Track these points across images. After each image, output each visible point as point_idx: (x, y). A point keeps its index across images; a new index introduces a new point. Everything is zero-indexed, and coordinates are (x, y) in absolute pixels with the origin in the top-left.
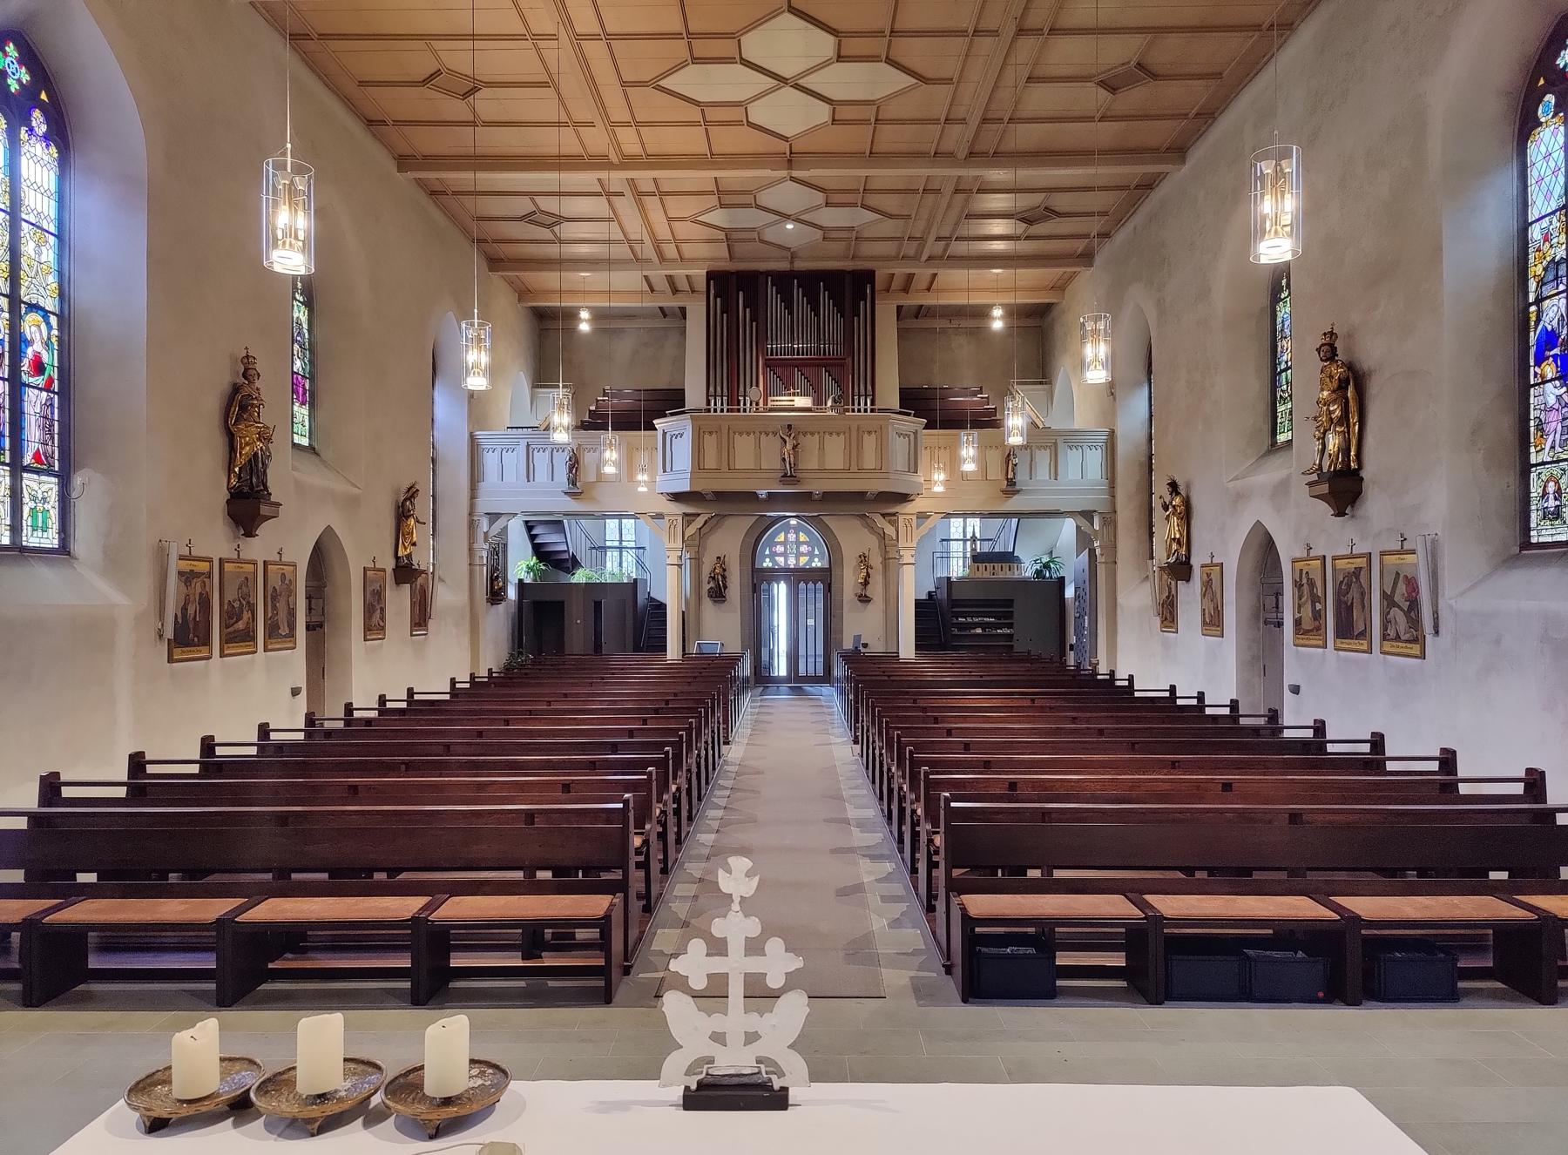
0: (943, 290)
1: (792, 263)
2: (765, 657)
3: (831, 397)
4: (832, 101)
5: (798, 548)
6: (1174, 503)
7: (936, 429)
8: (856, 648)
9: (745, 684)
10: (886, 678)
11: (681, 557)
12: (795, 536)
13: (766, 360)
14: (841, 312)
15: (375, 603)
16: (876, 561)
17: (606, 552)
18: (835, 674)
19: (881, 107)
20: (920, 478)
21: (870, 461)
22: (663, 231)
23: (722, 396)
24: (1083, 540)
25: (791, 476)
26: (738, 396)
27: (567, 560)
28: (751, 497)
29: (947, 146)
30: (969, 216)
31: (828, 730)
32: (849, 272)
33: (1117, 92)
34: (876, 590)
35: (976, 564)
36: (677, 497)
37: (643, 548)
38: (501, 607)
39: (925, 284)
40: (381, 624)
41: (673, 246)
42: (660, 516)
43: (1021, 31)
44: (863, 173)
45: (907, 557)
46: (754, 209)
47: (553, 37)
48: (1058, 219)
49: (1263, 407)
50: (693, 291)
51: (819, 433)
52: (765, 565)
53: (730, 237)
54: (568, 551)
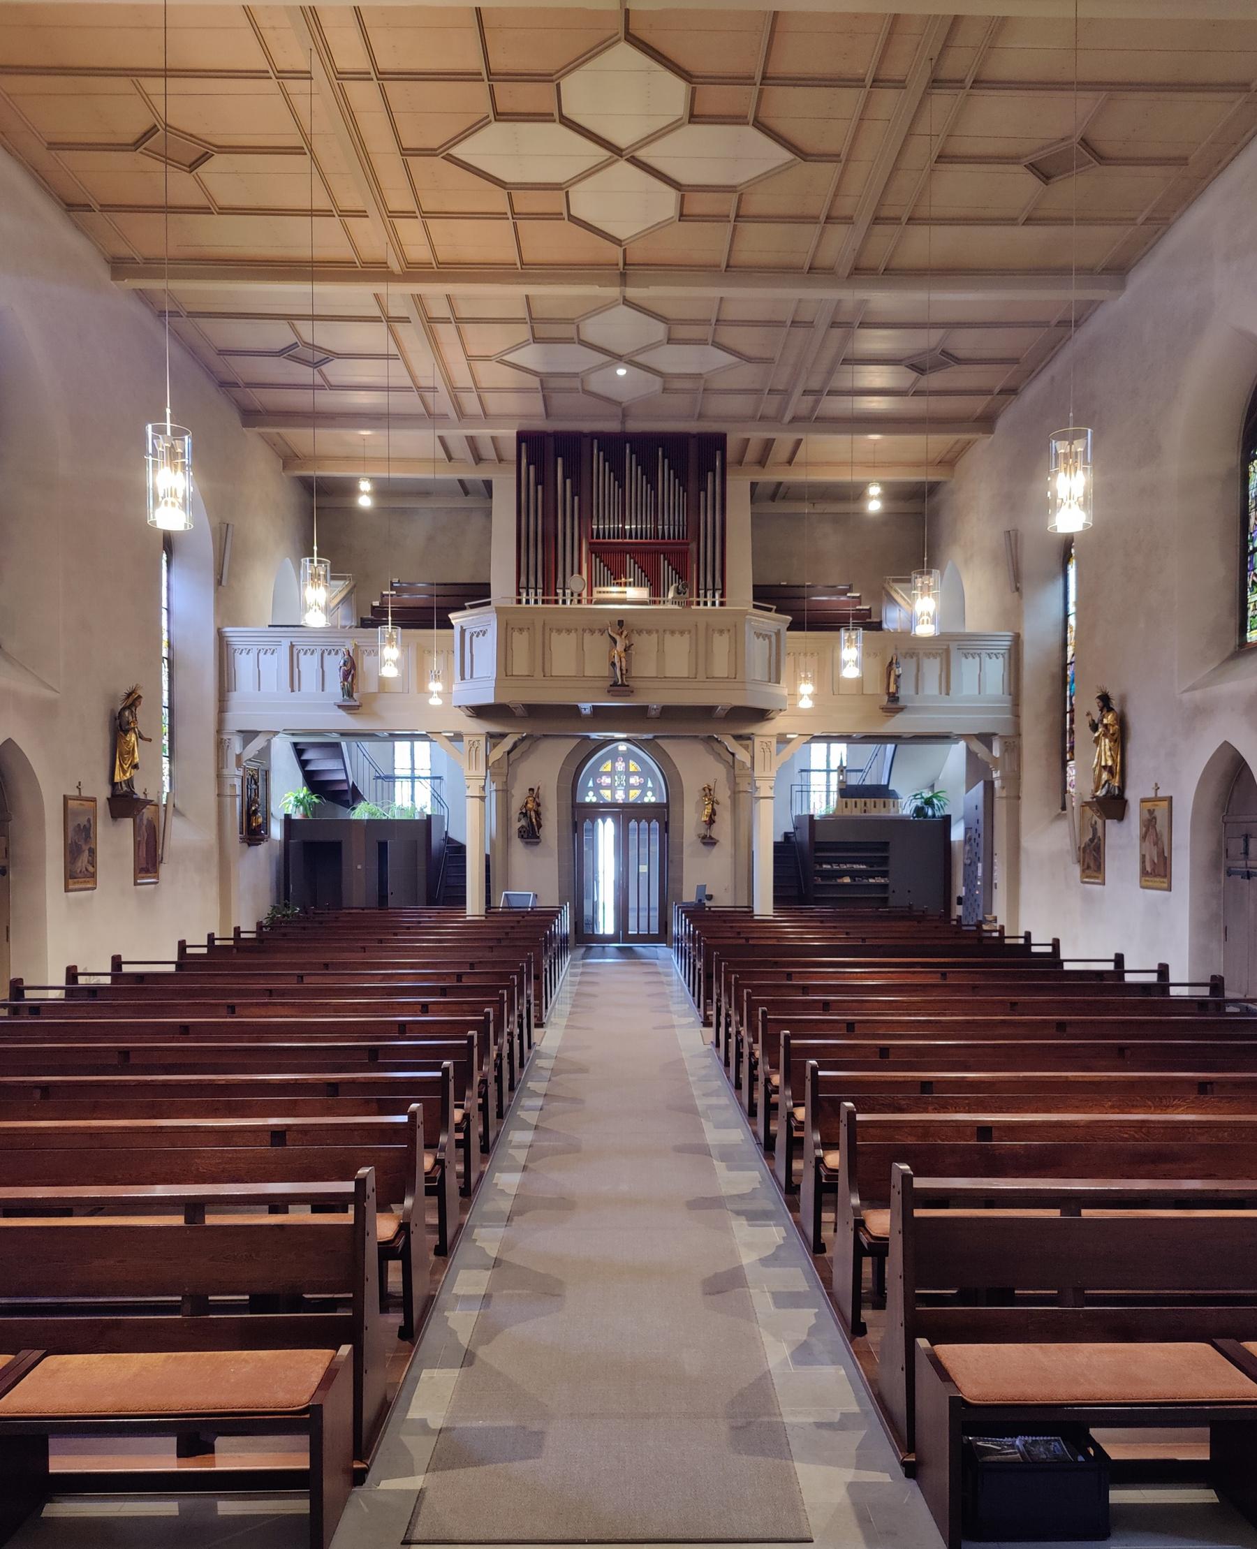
1: (623, 422)
2: (587, 911)
3: (674, 585)
4: (681, 185)
6: (1105, 721)
7: (804, 630)
8: (700, 901)
9: (564, 945)
10: (743, 941)
11: (483, 788)
12: (624, 765)
14: (684, 484)
15: (81, 843)
16: (723, 794)
17: (394, 782)
18: (675, 929)
19: (744, 196)
20: (783, 689)
21: (721, 667)
22: (462, 377)
23: (536, 589)
24: (977, 769)
25: (623, 685)
27: (346, 791)
28: (571, 712)
29: (828, 256)
30: (846, 361)
31: (667, 1006)
33: (1051, 181)
34: (723, 829)
35: (844, 800)
36: (479, 712)
37: (440, 778)
38: (262, 848)
40: (91, 869)
41: (474, 395)
42: (458, 737)
43: (936, 82)
44: (715, 292)
45: (765, 789)
47: (306, 75)
48: (957, 367)
49: (1229, 596)
50: (501, 460)
52: (587, 800)
53: (547, 385)
54: (346, 781)
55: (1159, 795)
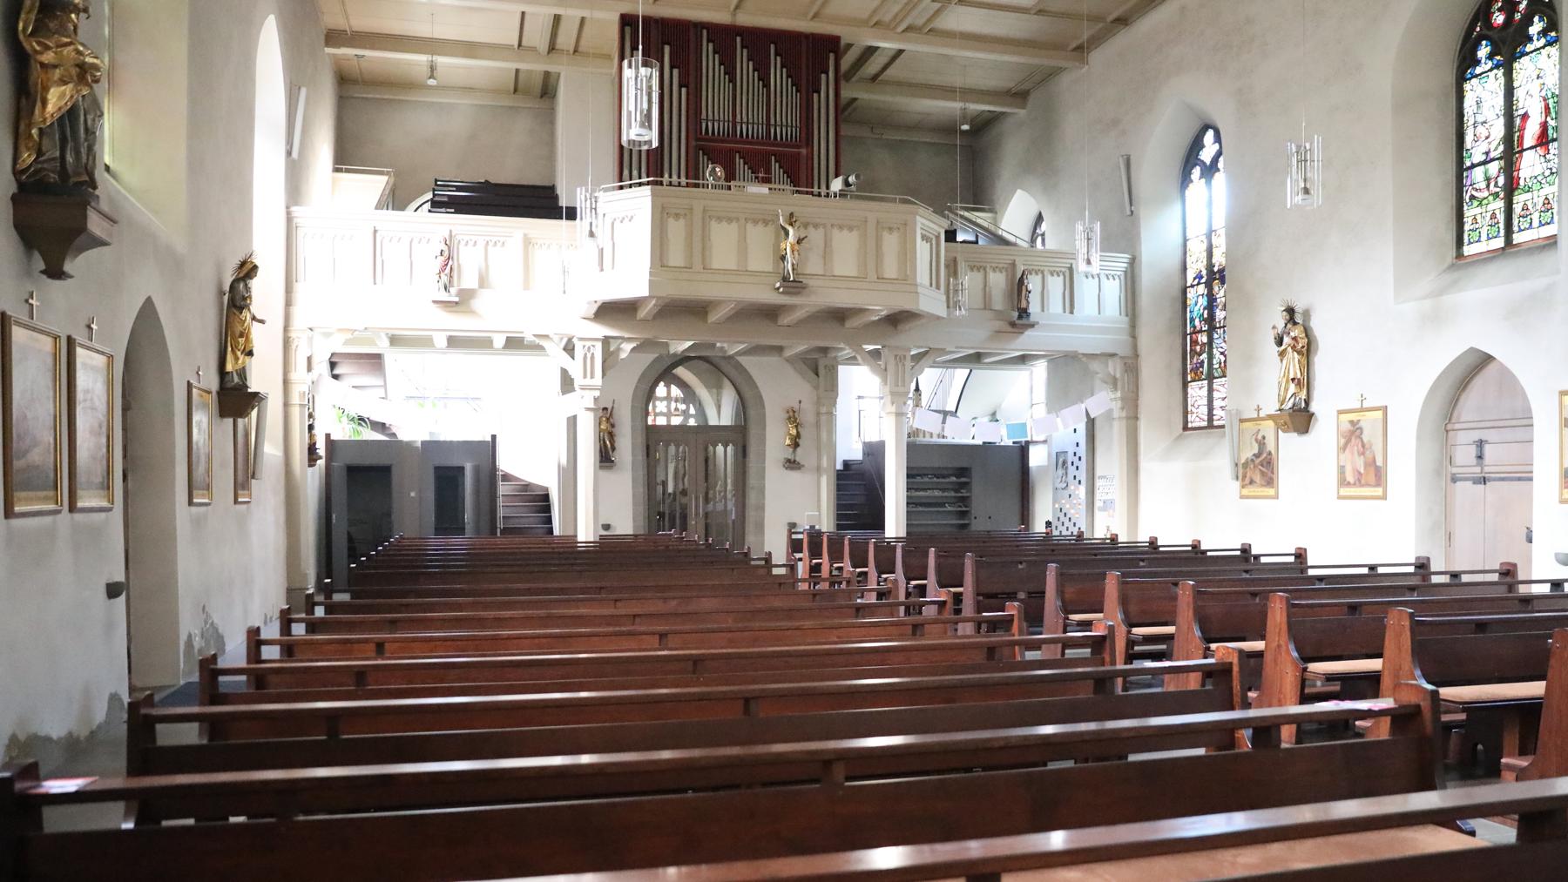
16: (808, 417)
55: (1364, 406)
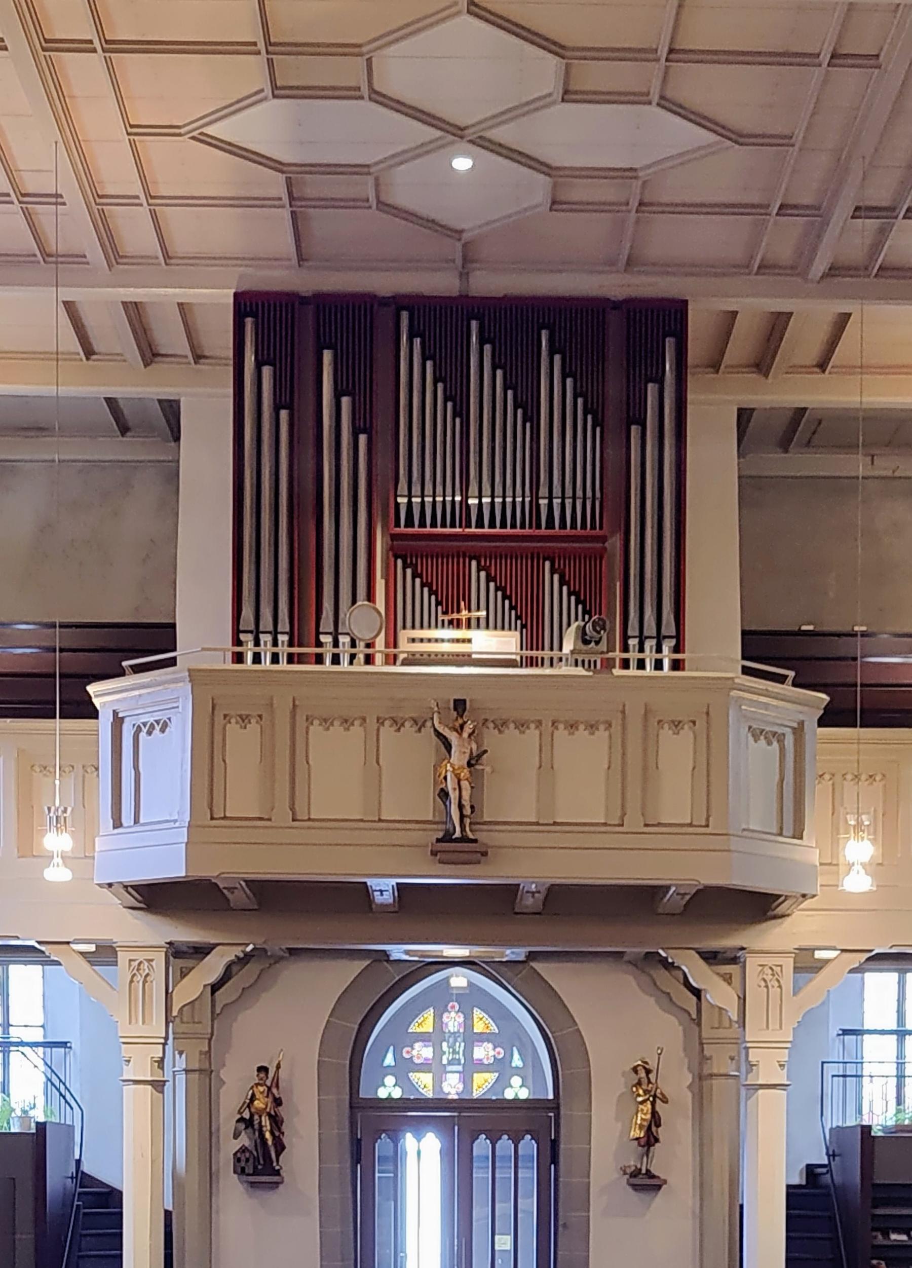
0: (863, 368)
1: (464, 275)
3: (574, 626)
5: (468, 1052)
11: (161, 1062)
13: (394, 537)
23: (275, 633)
25: (464, 839)
26: (318, 633)
32: (617, 305)
37: (64, 1045)
39: (812, 351)
46: (365, 104)
50: (198, 357)
51: (539, 723)
52: (382, 1093)
